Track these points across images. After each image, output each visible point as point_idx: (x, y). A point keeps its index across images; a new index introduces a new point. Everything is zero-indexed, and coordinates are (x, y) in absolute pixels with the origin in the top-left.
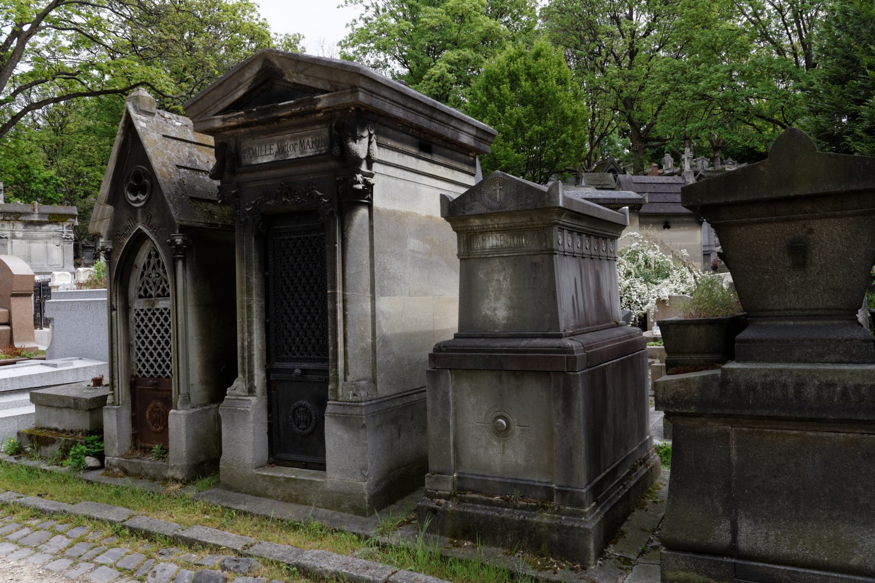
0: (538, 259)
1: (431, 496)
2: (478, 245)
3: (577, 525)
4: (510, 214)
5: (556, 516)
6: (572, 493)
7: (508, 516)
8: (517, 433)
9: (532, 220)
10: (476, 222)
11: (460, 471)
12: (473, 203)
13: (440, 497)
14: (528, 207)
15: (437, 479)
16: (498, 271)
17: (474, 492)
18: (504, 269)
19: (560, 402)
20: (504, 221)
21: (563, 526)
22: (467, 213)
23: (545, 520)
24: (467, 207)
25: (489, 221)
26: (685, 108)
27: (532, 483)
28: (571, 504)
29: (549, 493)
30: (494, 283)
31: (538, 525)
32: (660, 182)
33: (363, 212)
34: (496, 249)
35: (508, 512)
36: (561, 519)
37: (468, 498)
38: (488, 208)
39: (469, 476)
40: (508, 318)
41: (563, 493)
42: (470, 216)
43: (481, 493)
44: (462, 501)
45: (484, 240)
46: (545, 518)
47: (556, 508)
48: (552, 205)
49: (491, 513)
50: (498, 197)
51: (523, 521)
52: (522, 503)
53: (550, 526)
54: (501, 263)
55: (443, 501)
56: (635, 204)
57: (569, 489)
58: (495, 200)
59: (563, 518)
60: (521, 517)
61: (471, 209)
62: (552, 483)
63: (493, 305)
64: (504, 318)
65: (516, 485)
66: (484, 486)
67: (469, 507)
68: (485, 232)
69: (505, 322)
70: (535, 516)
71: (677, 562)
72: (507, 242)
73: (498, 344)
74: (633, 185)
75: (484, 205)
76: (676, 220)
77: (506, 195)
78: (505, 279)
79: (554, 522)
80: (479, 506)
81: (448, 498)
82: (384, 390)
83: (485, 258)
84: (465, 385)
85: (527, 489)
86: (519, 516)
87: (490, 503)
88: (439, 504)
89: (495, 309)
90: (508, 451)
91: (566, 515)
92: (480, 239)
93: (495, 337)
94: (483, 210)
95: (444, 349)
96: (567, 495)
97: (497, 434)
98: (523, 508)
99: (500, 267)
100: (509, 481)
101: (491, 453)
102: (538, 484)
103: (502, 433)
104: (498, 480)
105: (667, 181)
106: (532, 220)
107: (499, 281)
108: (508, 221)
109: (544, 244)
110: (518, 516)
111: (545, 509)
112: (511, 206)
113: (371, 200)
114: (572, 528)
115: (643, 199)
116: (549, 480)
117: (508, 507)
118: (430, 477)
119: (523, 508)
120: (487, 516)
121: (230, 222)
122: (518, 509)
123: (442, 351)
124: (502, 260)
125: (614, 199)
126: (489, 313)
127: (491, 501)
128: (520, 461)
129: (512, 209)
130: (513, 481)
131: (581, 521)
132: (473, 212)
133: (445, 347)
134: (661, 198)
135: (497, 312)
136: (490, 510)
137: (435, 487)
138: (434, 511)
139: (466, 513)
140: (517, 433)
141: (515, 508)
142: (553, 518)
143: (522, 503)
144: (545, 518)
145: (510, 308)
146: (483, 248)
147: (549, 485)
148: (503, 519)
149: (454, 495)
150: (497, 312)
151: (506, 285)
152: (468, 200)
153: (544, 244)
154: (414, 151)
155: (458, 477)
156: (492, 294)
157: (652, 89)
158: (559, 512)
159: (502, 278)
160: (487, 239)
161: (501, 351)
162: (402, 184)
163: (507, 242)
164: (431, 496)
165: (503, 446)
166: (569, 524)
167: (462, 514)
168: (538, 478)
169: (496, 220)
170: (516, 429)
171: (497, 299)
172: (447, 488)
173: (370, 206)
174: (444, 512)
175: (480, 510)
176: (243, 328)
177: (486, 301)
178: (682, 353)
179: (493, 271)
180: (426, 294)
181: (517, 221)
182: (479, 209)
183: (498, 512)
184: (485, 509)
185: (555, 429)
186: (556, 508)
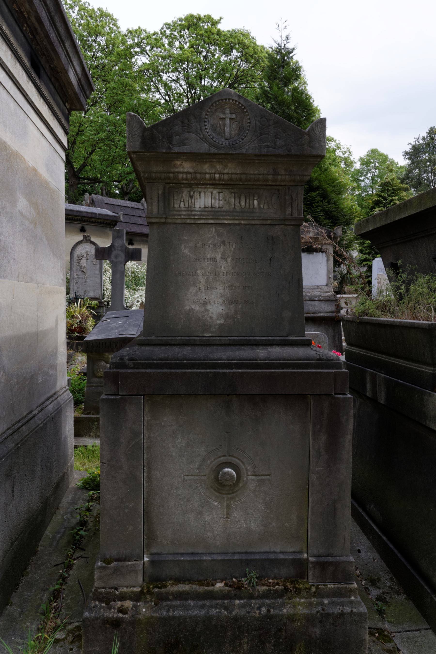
0: (277, 231)
1: (107, 599)
2: (181, 203)
3: (347, 609)
4: (243, 159)
5: (314, 600)
6: (336, 564)
7: (243, 612)
8: (252, 486)
9: (275, 173)
10: (186, 167)
11: (154, 550)
12: (187, 135)
13: (123, 597)
14: (278, 152)
15: (117, 570)
16: (214, 245)
17: (178, 580)
18: (223, 243)
19: (323, 438)
20: (231, 169)
21: (329, 615)
22: (176, 149)
23: (301, 610)
24: (176, 139)
25: (206, 168)
26: (117, 155)
27: (272, 556)
28: (334, 580)
29: (300, 568)
30: (205, 264)
31: (291, 618)
32: (125, 205)
34: (213, 212)
35: (242, 606)
36: (322, 604)
37: (173, 594)
38: (211, 145)
39: (170, 558)
40: (227, 317)
41: (322, 566)
42: (179, 156)
43: (190, 581)
44: (161, 598)
45: (191, 197)
46: (299, 607)
47: (313, 589)
48: (315, 153)
49: (214, 612)
50: (227, 130)
51: (268, 616)
52: (262, 588)
53: (309, 619)
54: (220, 235)
55: (128, 604)
56: (112, 221)
57: (331, 559)
58: (222, 134)
59: (326, 601)
60: (264, 610)
61: (182, 143)
62: (301, 552)
63: (203, 297)
64: (220, 316)
65: (248, 562)
66: (197, 571)
67: (175, 607)
68: (196, 184)
69: (222, 321)
70: (283, 605)
72: (229, 203)
73: (223, 354)
74: (104, 205)
75: (204, 139)
76: (138, 238)
77: (241, 129)
78: (224, 258)
79: (314, 611)
80: (191, 603)
81: (136, 598)
83: (193, 223)
84: (168, 419)
85: (265, 565)
86: (259, 608)
87: (211, 596)
88: (122, 610)
89: (206, 303)
90: (235, 514)
91: (328, 596)
92: (185, 195)
93: (207, 344)
94: (204, 148)
95: (131, 364)
96: (330, 569)
98: (265, 595)
99: (217, 240)
100: (236, 557)
101: (207, 518)
102: (281, 556)
103: (224, 487)
104: (219, 558)
105: (130, 206)
106: (275, 173)
107: (214, 260)
108: (239, 171)
109: (289, 211)
110: (259, 610)
111: (298, 592)
112: (250, 147)
114: (342, 614)
115: (119, 217)
116: (297, 549)
117: (240, 598)
118: (101, 568)
119: (265, 595)
120: (210, 618)
122: (257, 598)
123: (126, 367)
124: (221, 230)
125: (96, 214)
126: (197, 308)
127: (211, 592)
128: (253, 526)
129: (251, 152)
130: (244, 557)
131: (352, 602)
132: (186, 149)
133: (131, 359)
134: (133, 220)
135: (209, 307)
136: (211, 606)
137: (114, 582)
138: (116, 624)
139: (174, 618)
140: (252, 486)
141: (251, 597)
142: (311, 604)
143: (262, 588)
144: (299, 607)
145: (232, 301)
146: (190, 209)
147: (298, 556)
148: (236, 619)
149: (149, 592)
150: (209, 307)
151: (225, 267)
152: (177, 128)
153: (289, 211)
154: (26, 61)
155: (152, 562)
156: (202, 279)
157: (91, 135)
158: (319, 594)
159: (219, 257)
160: (196, 195)
161: (228, 366)
162: (13, 105)
163: (229, 203)
164: (107, 599)
165: (228, 507)
166: (337, 610)
167: (165, 621)
168: (282, 548)
169: (219, 167)
170: (251, 481)
171: (210, 287)
172: (135, 582)
174: (135, 622)
175: (195, 611)
176: (407, 364)
177: (193, 290)
179: (204, 245)
180: (31, 280)
182: (195, 145)
183: (226, 608)
184: (203, 607)
185: (313, 477)
186: (313, 589)
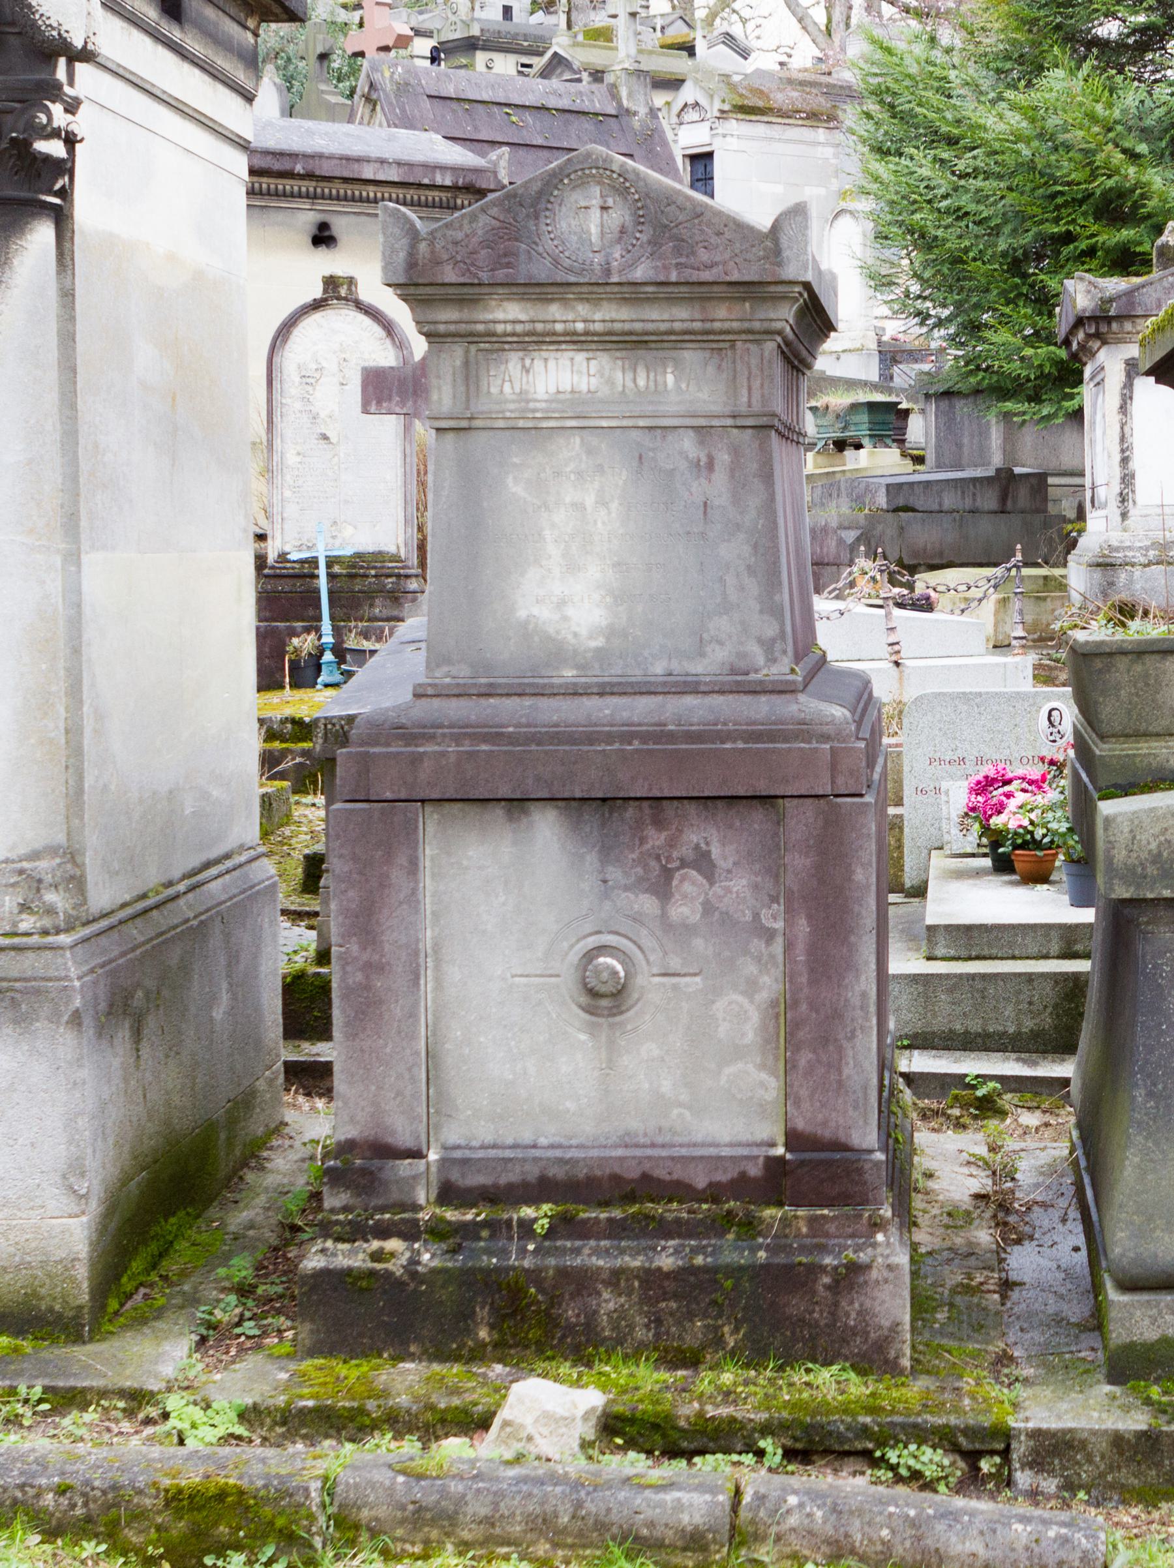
4: (632, 293)
16: (579, 474)
18: (600, 469)
25: (555, 311)
30: (560, 516)
33: (42, 234)
40: (611, 632)
54: (590, 452)
69: (599, 642)
71: (1154, 1320)
72: (610, 382)
78: (602, 502)
82: (104, 894)
83: (531, 429)
89: (562, 603)
97: (590, 1010)
107: (579, 507)
113: (65, 194)
121: (572, 477)
124: (593, 440)
150: (570, 611)
159: (590, 500)
163: (610, 382)
169: (583, 309)
171: (572, 567)
173: (61, 218)
177: (533, 574)
178: (1147, 735)
181: (656, 316)
